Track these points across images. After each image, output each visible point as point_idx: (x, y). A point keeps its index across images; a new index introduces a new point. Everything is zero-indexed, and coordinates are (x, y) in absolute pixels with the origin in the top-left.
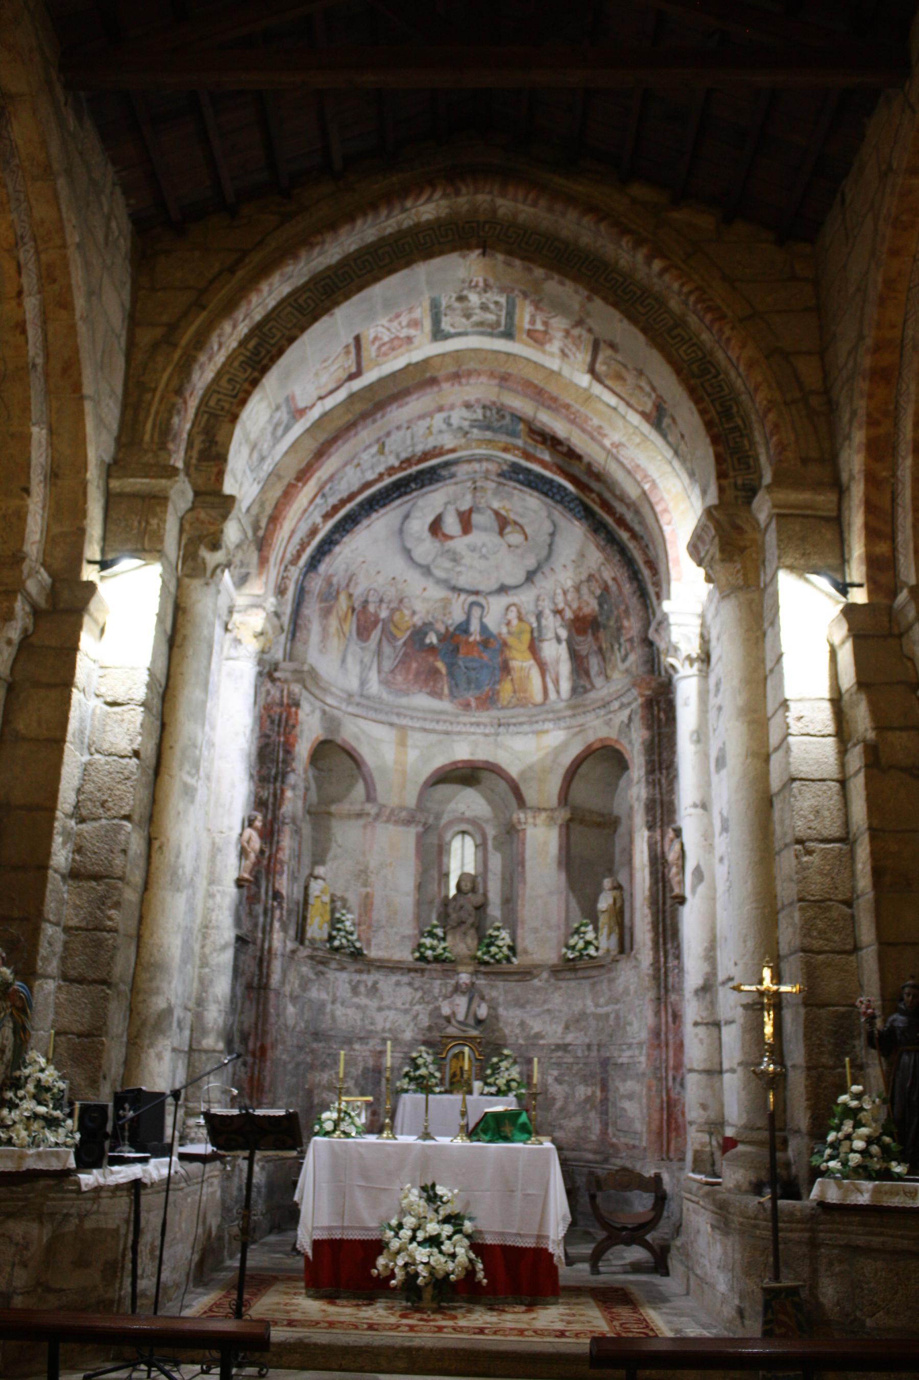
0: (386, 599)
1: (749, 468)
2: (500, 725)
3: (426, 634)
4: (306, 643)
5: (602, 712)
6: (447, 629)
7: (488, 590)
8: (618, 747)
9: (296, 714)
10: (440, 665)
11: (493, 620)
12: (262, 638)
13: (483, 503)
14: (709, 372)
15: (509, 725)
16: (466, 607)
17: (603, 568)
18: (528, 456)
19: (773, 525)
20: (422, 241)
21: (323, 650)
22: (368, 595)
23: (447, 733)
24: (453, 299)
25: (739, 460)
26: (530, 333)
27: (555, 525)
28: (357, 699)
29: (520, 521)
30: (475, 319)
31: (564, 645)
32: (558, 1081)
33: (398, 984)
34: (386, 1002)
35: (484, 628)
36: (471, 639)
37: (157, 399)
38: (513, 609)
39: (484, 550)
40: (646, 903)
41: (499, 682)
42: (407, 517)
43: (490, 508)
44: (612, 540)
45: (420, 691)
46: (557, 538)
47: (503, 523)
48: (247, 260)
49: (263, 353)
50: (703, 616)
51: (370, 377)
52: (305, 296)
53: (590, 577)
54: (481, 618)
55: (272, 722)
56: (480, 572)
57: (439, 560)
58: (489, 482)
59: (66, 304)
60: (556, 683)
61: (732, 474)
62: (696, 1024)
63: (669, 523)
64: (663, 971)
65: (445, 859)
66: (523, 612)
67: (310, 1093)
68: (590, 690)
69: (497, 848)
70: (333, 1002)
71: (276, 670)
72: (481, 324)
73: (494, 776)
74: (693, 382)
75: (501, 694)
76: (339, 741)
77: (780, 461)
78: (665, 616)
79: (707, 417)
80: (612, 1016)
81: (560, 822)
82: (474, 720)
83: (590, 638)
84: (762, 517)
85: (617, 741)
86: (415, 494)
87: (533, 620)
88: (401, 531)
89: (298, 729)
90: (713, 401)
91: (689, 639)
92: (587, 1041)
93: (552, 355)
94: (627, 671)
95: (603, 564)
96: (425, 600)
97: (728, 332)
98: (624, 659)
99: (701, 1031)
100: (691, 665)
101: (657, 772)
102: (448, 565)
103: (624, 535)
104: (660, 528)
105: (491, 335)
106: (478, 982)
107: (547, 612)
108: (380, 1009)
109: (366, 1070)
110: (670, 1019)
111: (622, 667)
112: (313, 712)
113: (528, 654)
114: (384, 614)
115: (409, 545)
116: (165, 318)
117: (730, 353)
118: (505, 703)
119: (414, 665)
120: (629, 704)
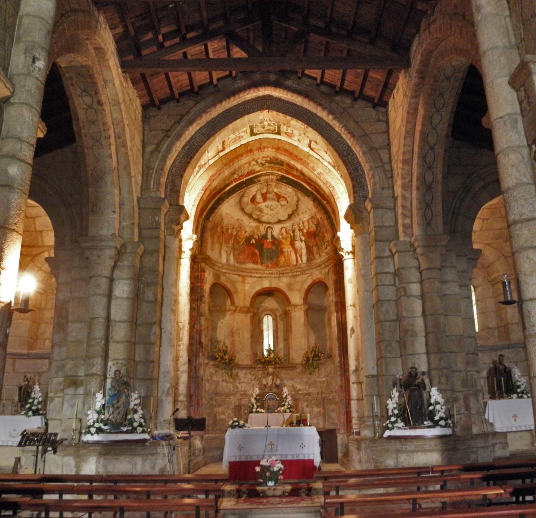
4: (206, 247)
5: (318, 268)
6: (259, 237)
8: (324, 281)
11: (275, 234)
13: (271, 190)
18: (287, 173)
19: (372, 212)
21: (212, 249)
23: (260, 277)
25: (361, 186)
26: (286, 133)
28: (226, 266)
29: (285, 196)
30: (266, 128)
31: (303, 242)
32: (307, 406)
34: (242, 380)
35: (273, 236)
36: (268, 241)
37: (154, 172)
38: (283, 229)
39: (272, 207)
40: (336, 340)
41: (279, 257)
42: (242, 197)
43: (273, 191)
46: (300, 203)
47: (279, 197)
48: (184, 118)
49: (191, 151)
51: (227, 150)
53: (312, 217)
54: (272, 233)
56: (271, 215)
59: (124, 146)
60: (301, 257)
61: (358, 192)
62: (353, 383)
65: (261, 325)
67: (215, 416)
72: (269, 130)
74: (344, 158)
77: (374, 189)
78: (338, 238)
79: (350, 171)
82: (270, 272)
83: (313, 240)
84: (369, 208)
85: (324, 279)
87: (291, 233)
92: (317, 391)
93: (295, 141)
96: (249, 226)
98: (326, 249)
102: (258, 213)
105: (272, 133)
107: (297, 230)
108: (240, 383)
109: (235, 406)
111: (325, 251)
112: (210, 273)
113: (290, 246)
114: (234, 233)
115: (243, 207)
116: (155, 141)
119: (247, 252)
120: (328, 266)
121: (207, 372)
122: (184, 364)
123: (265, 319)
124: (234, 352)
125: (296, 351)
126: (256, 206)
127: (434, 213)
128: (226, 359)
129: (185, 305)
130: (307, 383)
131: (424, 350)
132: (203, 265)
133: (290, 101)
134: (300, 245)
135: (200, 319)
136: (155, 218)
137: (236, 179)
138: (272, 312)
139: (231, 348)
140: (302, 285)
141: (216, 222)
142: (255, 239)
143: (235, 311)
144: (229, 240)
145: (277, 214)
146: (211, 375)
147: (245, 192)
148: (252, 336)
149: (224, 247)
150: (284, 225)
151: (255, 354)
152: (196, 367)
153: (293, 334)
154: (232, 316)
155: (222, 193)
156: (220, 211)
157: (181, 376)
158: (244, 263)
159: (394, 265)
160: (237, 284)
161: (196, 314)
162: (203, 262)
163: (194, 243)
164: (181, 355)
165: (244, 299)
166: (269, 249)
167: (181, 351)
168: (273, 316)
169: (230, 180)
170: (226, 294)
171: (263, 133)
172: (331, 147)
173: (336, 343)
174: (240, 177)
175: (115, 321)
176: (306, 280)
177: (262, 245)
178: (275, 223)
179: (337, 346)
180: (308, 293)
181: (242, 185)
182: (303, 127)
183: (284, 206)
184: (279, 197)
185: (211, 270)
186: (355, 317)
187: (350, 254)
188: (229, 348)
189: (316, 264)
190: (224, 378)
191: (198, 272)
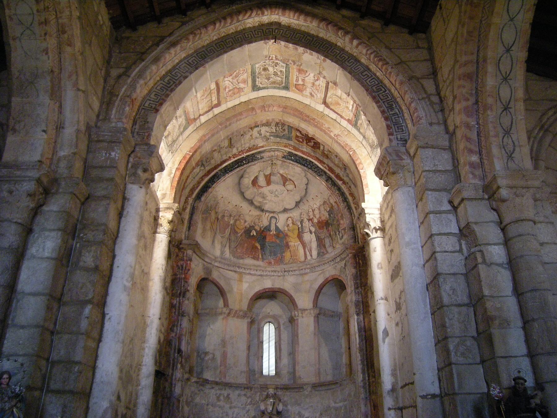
0: (233, 215)
1: (403, 131)
3: (251, 232)
6: (260, 229)
7: (278, 211)
9: (190, 264)
10: (258, 245)
11: (280, 225)
12: (172, 224)
14: (381, 90)
16: (269, 219)
17: (330, 198)
18: (295, 149)
20: (247, 36)
21: (203, 236)
22: (224, 213)
24: (262, 69)
29: (292, 179)
31: (313, 233)
33: (239, 395)
34: (233, 405)
35: (277, 228)
36: (272, 233)
38: (290, 219)
41: (284, 252)
42: (242, 177)
44: (334, 184)
47: (285, 180)
48: (165, 40)
50: (381, 209)
51: (223, 107)
52: (192, 59)
53: (325, 203)
55: (179, 268)
58: (278, 161)
60: (310, 251)
61: (395, 134)
62: (390, 409)
63: (362, 169)
65: (261, 335)
68: (326, 254)
70: (208, 405)
71: (181, 244)
72: (274, 83)
73: (283, 295)
75: (285, 257)
76: (210, 278)
78: (363, 210)
79: (382, 109)
81: (314, 315)
82: (273, 269)
83: (325, 230)
85: (339, 276)
86: (245, 166)
87: (299, 224)
88: (239, 183)
89: (190, 272)
90: (383, 102)
93: (306, 96)
94: (343, 243)
97: (390, 70)
100: (376, 232)
101: (359, 288)
102: (260, 200)
103: (340, 183)
104: (359, 172)
105: (279, 88)
106: (277, 393)
107: (305, 220)
108: (231, 408)
111: (340, 242)
113: (297, 239)
114: (232, 222)
117: (391, 80)
118: (287, 261)
119: (246, 245)
120: (345, 258)
126: (258, 191)
127: (516, 143)
129: (156, 294)
131: (524, 350)
132: (190, 252)
133: (303, 29)
134: (310, 238)
136: (110, 154)
137: (235, 154)
138: (274, 320)
141: (209, 205)
142: (256, 230)
149: (218, 237)
150: (291, 215)
155: (217, 170)
156: (214, 193)
158: (242, 258)
159: (458, 221)
164: (144, 363)
167: (145, 357)
169: (228, 156)
170: (219, 294)
171: (267, 88)
172: (356, 83)
173: (358, 354)
174: (239, 152)
175: (23, 292)
176: (316, 280)
177: (265, 238)
179: (359, 358)
180: (319, 295)
181: (242, 162)
182: (319, 61)
184: (285, 180)
185: (201, 261)
186: (388, 315)
187: (379, 231)
189: (329, 258)
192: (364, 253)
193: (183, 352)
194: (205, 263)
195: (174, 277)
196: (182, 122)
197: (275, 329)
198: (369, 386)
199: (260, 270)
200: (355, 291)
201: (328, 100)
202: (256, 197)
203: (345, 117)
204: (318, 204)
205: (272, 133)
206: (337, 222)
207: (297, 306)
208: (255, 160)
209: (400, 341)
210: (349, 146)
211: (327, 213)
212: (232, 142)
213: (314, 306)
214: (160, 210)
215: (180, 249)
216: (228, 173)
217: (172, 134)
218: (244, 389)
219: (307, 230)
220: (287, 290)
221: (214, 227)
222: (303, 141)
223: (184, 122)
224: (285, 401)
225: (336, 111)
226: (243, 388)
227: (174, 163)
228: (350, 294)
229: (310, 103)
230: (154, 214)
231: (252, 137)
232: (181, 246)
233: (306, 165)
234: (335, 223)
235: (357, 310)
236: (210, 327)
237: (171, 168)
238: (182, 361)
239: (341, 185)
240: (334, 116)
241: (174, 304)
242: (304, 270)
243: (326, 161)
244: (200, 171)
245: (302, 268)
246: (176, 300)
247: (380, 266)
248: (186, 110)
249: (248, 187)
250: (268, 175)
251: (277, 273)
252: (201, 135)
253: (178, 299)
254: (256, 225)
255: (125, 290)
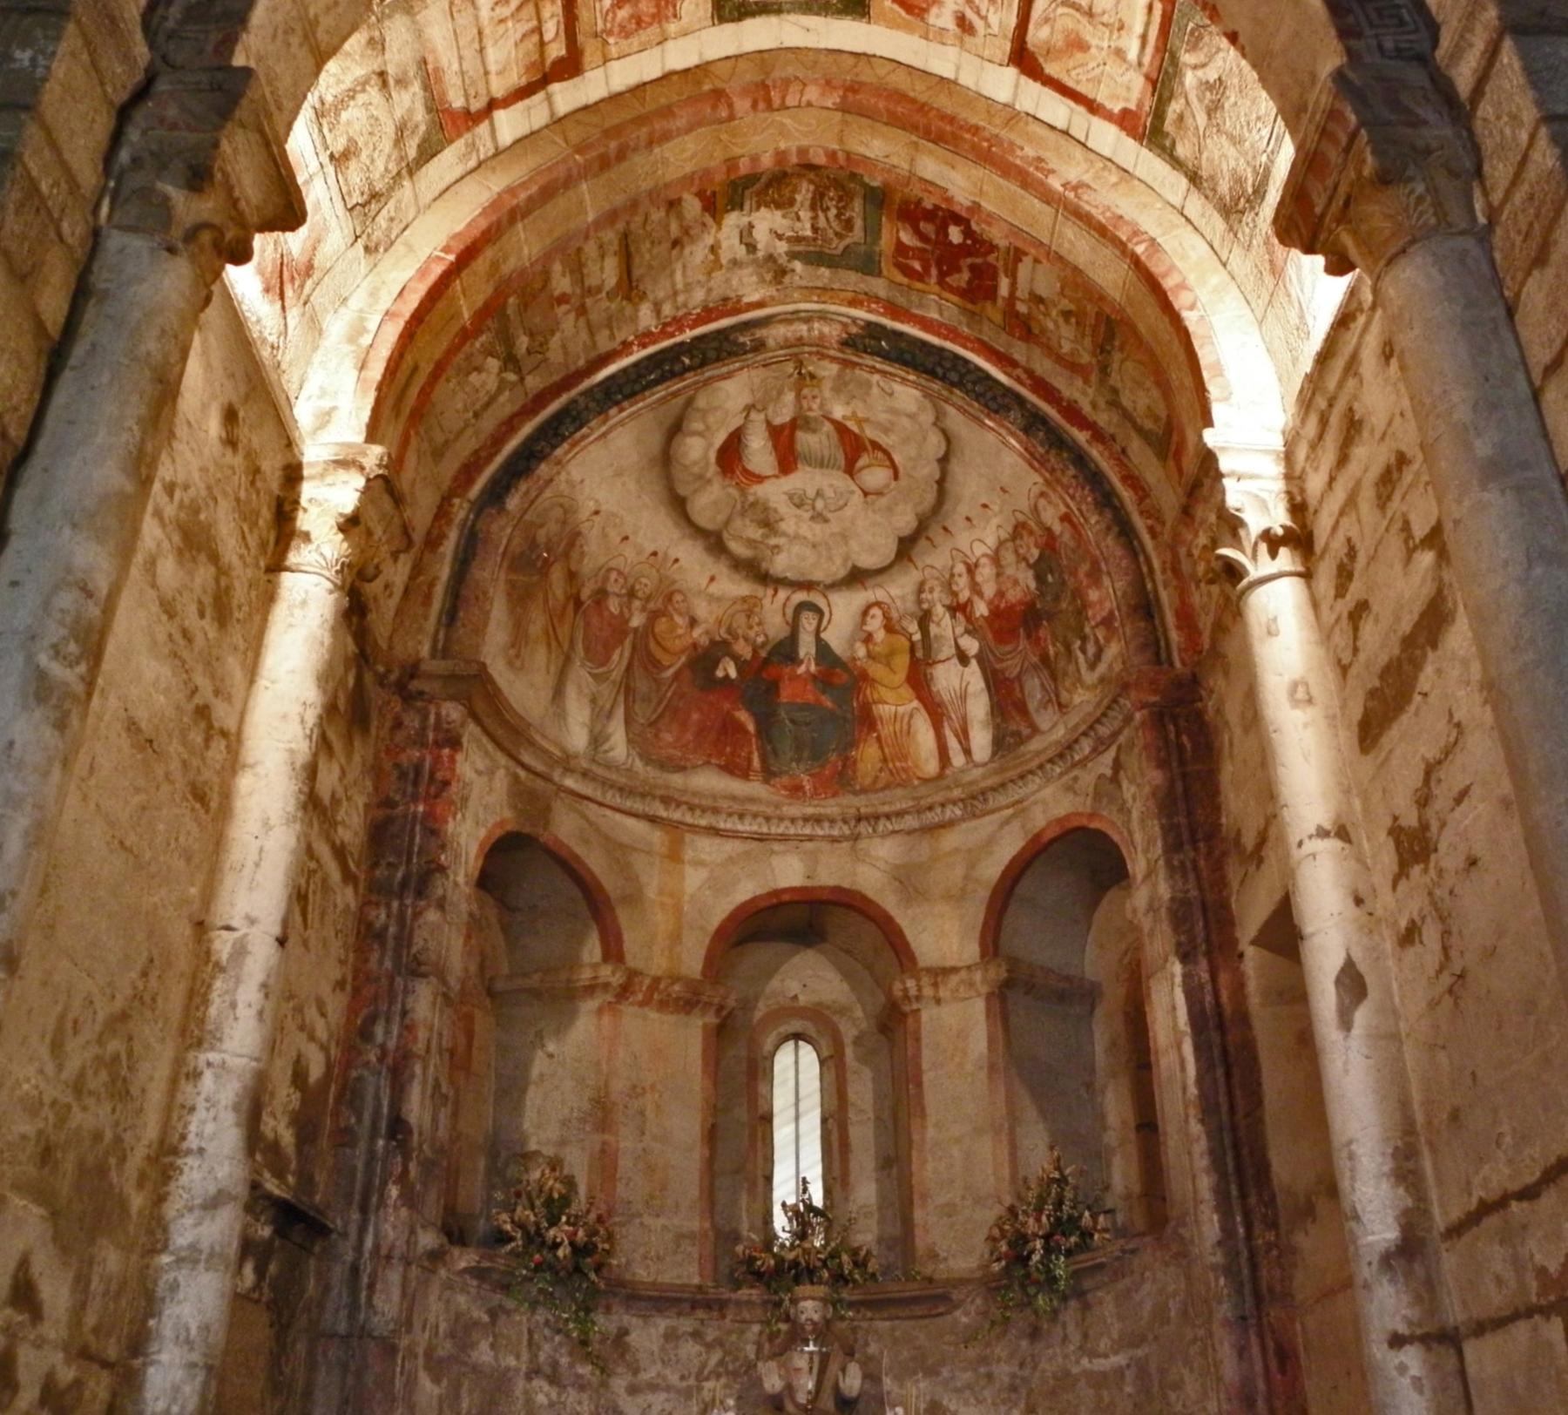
1: (1402, 23)
2: (859, 819)
6: (755, 651)
7: (828, 581)
9: (452, 760)
10: (744, 716)
11: (837, 636)
15: (877, 818)
16: (790, 612)
18: (895, 311)
21: (516, 661)
22: (606, 579)
23: (761, 838)
27: (948, 438)
31: (974, 663)
34: (644, 1376)
35: (823, 649)
36: (801, 670)
38: (876, 611)
41: (853, 744)
42: (675, 429)
44: (1058, 441)
45: (708, 763)
46: (955, 467)
50: (1289, 457)
53: (1019, 530)
57: (738, 523)
58: (826, 363)
60: (964, 735)
61: (1368, 32)
62: (1397, 1341)
63: (1192, 307)
64: (1245, 1254)
65: (762, 1089)
66: (895, 615)
68: (1030, 737)
69: (862, 1060)
71: (412, 676)
75: (860, 766)
76: (544, 838)
80: (1130, 1375)
81: (984, 989)
82: (810, 811)
83: (1023, 643)
85: (1092, 816)
86: (690, 378)
87: (913, 627)
91: (1263, 505)
94: (1102, 680)
95: (1042, 494)
96: (712, 599)
99: (1412, 1358)
100: (1273, 554)
101: (1187, 847)
102: (756, 533)
103: (1081, 437)
107: (939, 610)
108: (633, 1390)
110: (1274, 1365)
111: (1090, 678)
113: (907, 692)
114: (637, 621)
115: (682, 490)
118: (868, 781)
120: (1115, 735)
121: (435, 1309)
122: (213, 1204)
123: (784, 1060)
124: (610, 1212)
125: (950, 1210)
126: (743, 492)
128: (556, 1246)
129: (267, 826)
130: (1013, 1389)
132: (453, 712)
135: (406, 991)
139: (590, 1189)
140: (972, 866)
142: (736, 658)
143: (624, 992)
144: (608, 650)
145: (844, 537)
146: (463, 1332)
147: (689, 403)
148: (712, 1136)
149: (580, 675)
150: (880, 594)
151: (726, 1237)
152: (355, 1270)
153: (931, 1119)
154: (606, 1019)
155: (574, 392)
157: (174, 1287)
158: (682, 769)
160: (639, 862)
161: (388, 964)
162: (452, 698)
163: (366, 491)
164: (192, 1142)
165: (676, 938)
166: (806, 707)
167: (201, 1113)
168: (824, 1043)
169: (619, 339)
170: (582, 907)
173: (1196, 1128)
174: (665, 325)
176: (990, 843)
177: (773, 687)
178: (835, 586)
181: (677, 359)
183: (880, 494)
185: (502, 759)
186: (1359, 901)
188: (582, 1189)
189: (1038, 753)
190: (542, 1357)
191: (424, 745)
192: (1199, 705)
193: (410, 1132)
194: (522, 774)
195: (380, 814)
196: (410, 111)
197: (822, 1062)
198: (1254, 1267)
199: (755, 816)
200: (1169, 863)
201: (1037, 35)
202: (738, 523)
203: (1109, 105)
204: (991, 541)
205: (798, 239)
206: (1074, 598)
207: (912, 958)
208: (731, 354)
209: (1433, 1004)
210: (1127, 223)
211: (1030, 574)
212: (636, 273)
213: (983, 954)
214: (306, 472)
215: (408, 698)
216: (617, 403)
217: (364, 156)
218: (693, 1308)
219: (947, 650)
220: (870, 894)
221: (564, 632)
222: (926, 269)
223: (420, 115)
224: (871, 1358)
225: (1071, 84)
226: (686, 1306)
227: (374, 294)
228: (1148, 876)
229: (958, 68)
230: (277, 492)
231: (717, 260)
232: (415, 685)
233: (940, 371)
234: (1064, 605)
235: (1183, 938)
236: (543, 1046)
237: (361, 311)
238: (406, 1171)
239: (1086, 446)
240: (1056, 110)
241: (378, 925)
242: (939, 810)
243: (1019, 352)
244: (500, 390)
245: (930, 800)
246: (388, 906)
247: (1300, 695)
248: (430, 59)
249: (700, 477)
250: (783, 427)
251: (826, 825)
252: (496, 189)
253: (395, 904)
254: (736, 638)
255: (41, 699)
